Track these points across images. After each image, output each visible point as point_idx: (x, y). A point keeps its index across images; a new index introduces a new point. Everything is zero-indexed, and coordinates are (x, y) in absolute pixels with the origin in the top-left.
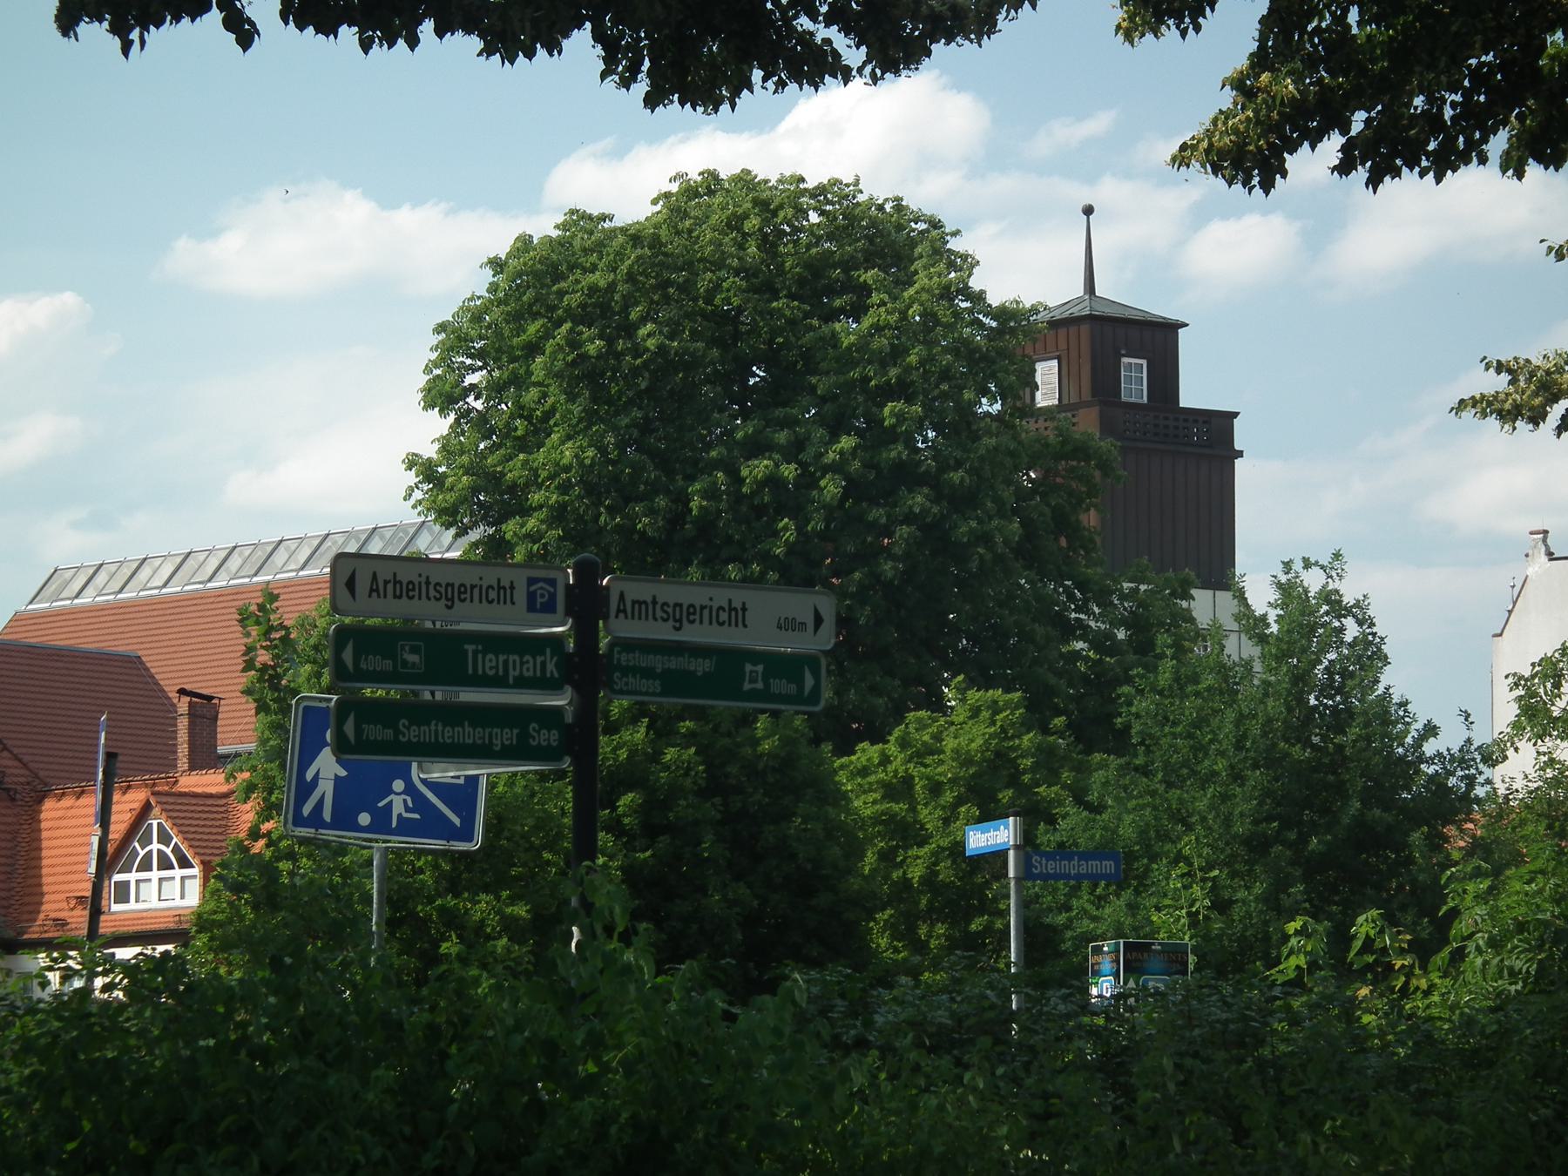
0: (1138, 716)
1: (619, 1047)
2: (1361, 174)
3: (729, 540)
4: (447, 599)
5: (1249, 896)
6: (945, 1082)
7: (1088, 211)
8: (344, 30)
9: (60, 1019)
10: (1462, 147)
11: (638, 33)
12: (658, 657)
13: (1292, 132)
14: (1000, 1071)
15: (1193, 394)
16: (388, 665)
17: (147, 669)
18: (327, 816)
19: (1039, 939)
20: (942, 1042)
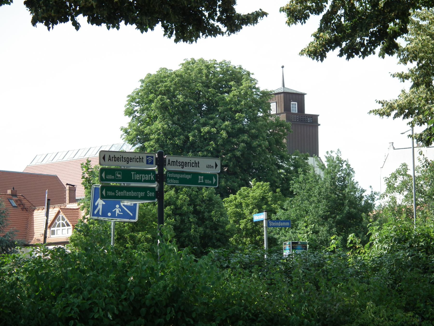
0: (295, 188)
1: (169, 268)
2: (345, 56)
3: (199, 147)
4: (182, 166)
5: (323, 229)
6: (247, 276)
7: (283, 67)
8: (103, 24)
9: (34, 263)
10: (369, 50)
11: (172, 25)
12: (178, 175)
13: (328, 47)
14: (260, 273)
15: (308, 111)
16: (113, 177)
17: (59, 179)
18: (100, 214)
19: (272, 241)
20: (247, 266)
